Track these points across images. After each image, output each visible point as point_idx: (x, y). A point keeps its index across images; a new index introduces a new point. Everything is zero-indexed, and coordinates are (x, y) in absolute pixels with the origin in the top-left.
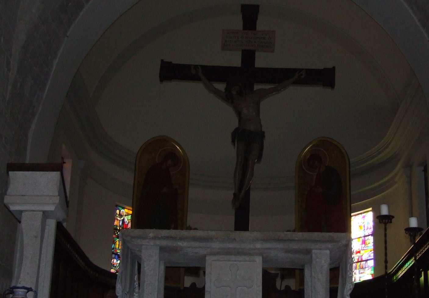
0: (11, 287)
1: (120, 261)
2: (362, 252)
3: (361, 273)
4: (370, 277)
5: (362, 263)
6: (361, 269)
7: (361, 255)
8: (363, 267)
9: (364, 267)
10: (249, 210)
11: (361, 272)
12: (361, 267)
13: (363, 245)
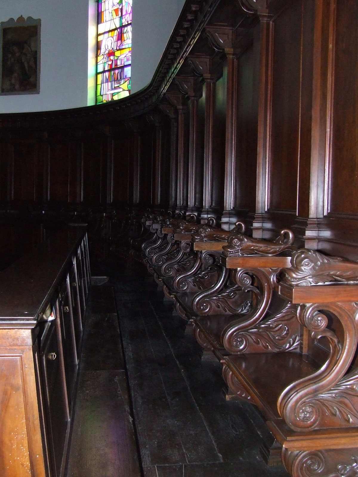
0: (130, 26)
1: (132, 27)
2: (117, 53)
3: (115, 88)
4: (126, 94)
5: (117, 71)
6: (114, 81)
7: (116, 58)
8: (118, 79)
9: (119, 78)
10: (256, 177)
11: (116, 86)
12: (114, 78)
13: (119, 42)
